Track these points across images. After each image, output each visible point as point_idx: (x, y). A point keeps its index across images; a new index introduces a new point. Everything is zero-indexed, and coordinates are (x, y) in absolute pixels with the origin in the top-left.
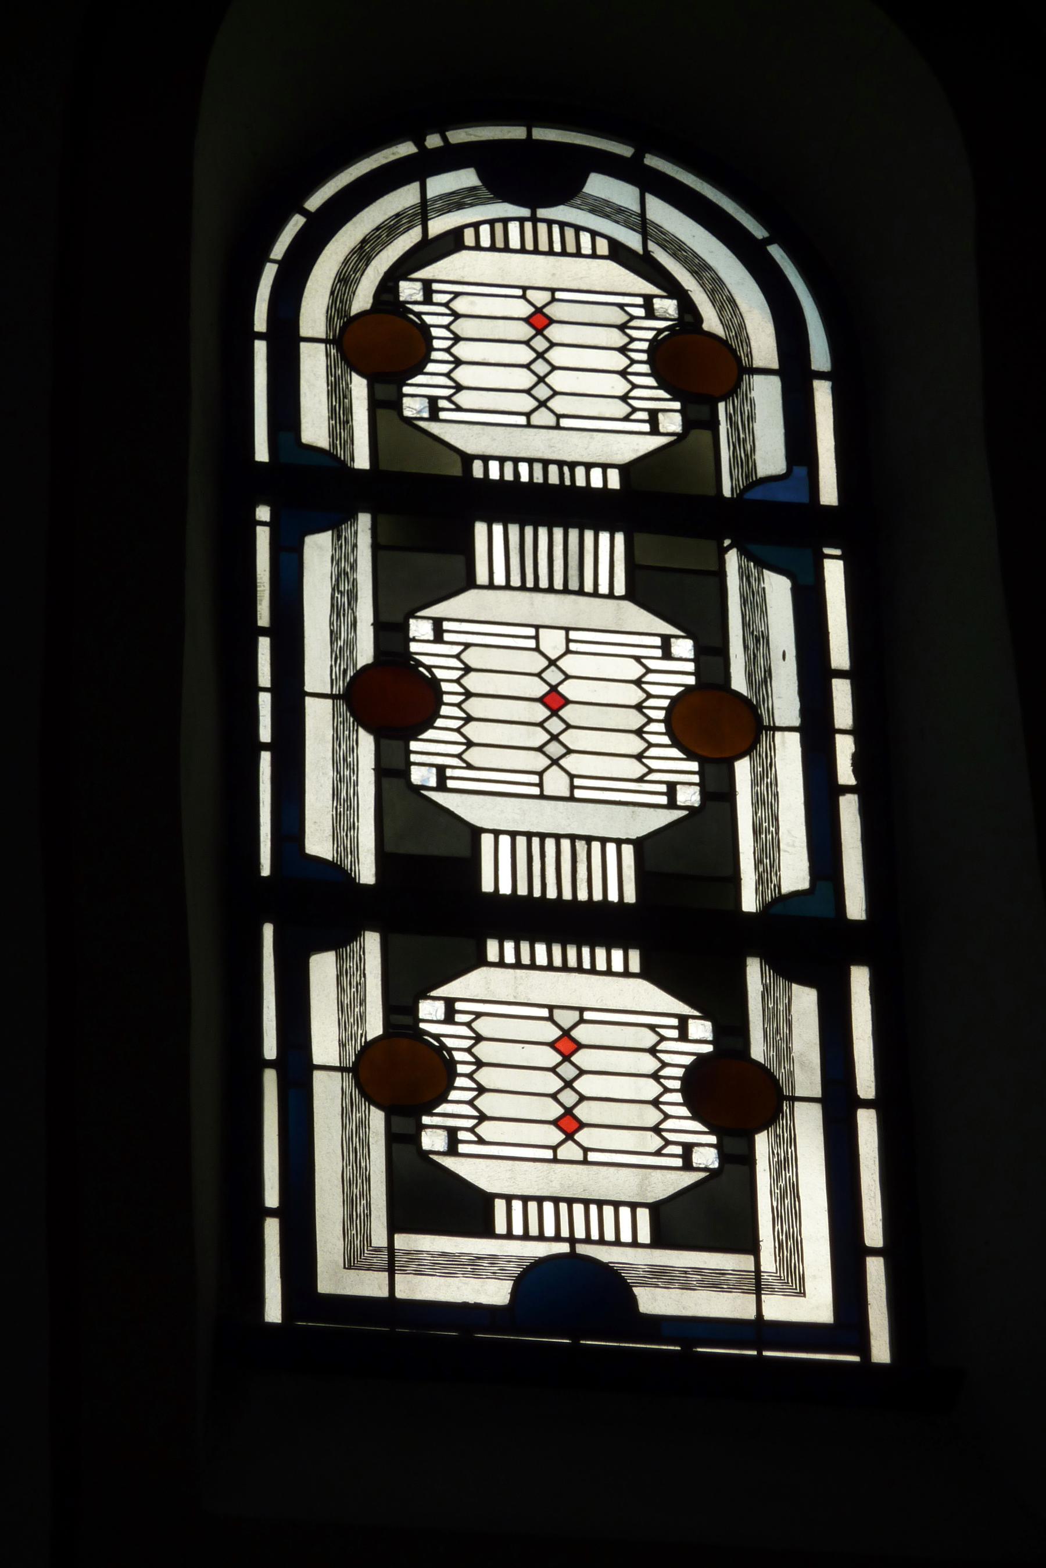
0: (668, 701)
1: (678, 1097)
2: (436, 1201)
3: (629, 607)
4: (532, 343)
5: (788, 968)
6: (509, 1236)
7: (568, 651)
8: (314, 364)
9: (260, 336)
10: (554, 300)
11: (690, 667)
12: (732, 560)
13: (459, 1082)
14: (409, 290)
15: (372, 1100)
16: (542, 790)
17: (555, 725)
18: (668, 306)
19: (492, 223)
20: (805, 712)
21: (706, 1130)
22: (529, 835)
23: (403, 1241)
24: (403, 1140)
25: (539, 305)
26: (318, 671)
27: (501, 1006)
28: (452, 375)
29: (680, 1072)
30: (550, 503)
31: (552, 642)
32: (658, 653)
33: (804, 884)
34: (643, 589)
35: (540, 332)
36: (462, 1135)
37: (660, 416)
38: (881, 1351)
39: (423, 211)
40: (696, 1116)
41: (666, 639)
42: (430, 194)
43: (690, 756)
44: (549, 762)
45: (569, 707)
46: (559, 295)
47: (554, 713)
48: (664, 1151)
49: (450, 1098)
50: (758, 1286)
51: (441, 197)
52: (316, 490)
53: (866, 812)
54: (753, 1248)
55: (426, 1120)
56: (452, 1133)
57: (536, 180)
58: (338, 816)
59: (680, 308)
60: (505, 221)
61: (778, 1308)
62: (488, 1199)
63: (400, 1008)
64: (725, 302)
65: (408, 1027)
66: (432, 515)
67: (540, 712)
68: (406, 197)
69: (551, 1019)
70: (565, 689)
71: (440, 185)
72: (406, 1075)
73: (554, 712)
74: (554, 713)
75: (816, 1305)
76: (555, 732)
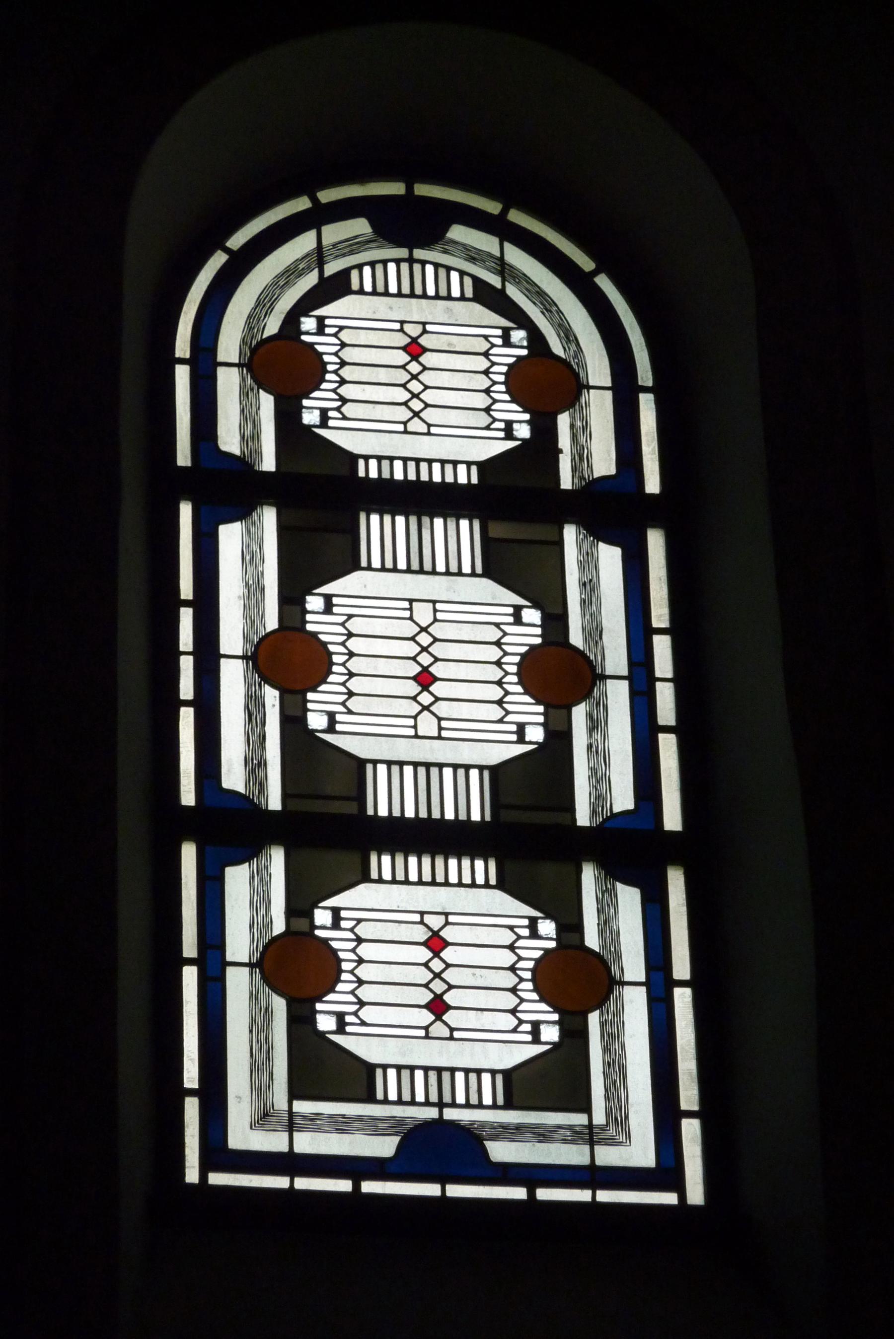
0: (533, 963)
1: (515, 679)
2: (325, 1070)
3: (498, 894)
4: (419, 698)
5: (615, 870)
6: (386, 1101)
7: (436, 620)
8: (229, 383)
9: (187, 603)
10: (447, 923)
11: (538, 631)
12: (589, 875)
13: (328, 377)
14: (308, 324)
15: (267, 679)
16: (416, 732)
17: (425, 659)
18: (519, 336)
19: (372, 264)
20: (632, 663)
21: (551, 1010)
22: (407, 882)
23: (302, 1107)
24: (301, 1019)
25: (436, 929)
26: (232, 637)
27: (381, 915)
28: (355, 930)
29: (517, 659)
30: (420, 499)
31: (423, 614)
32: (511, 619)
33: (630, 805)
34: (496, 565)
35: (425, 670)
36: (348, 1019)
37: (542, 1027)
38: (696, 1195)
39: (319, 256)
40: (527, 692)
41: (518, 609)
42: (325, 242)
43: (538, 702)
44: (412, 415)
45: (438, 683)
46: (451, 919)
47: (436, 954)
48: (492, 427)
49: (337, 989)
50: (590, 1136)
51: (334, 245)
52: (229, 489)
53: (658, 403)
54: (586, 1108)
55: (305, 402)
56: (331, 716)
57: (411, 227)
58: (246, 751)
59: (530, 339)
60: (385, 262)
61: (608, 1156)
62: (370, 1069)
63: (300, 907)
64: (568, 335)
65: (303, 934)
66: (326, 507)
67: (424, 954)
68: (305, 243)
69: (401, 330)
70: (448, 998)
71: (333, 233)
72: (300, 966)
73: (424, 666)
74: (436, 954)
75: (640, 1151)
76: (425, 645)
